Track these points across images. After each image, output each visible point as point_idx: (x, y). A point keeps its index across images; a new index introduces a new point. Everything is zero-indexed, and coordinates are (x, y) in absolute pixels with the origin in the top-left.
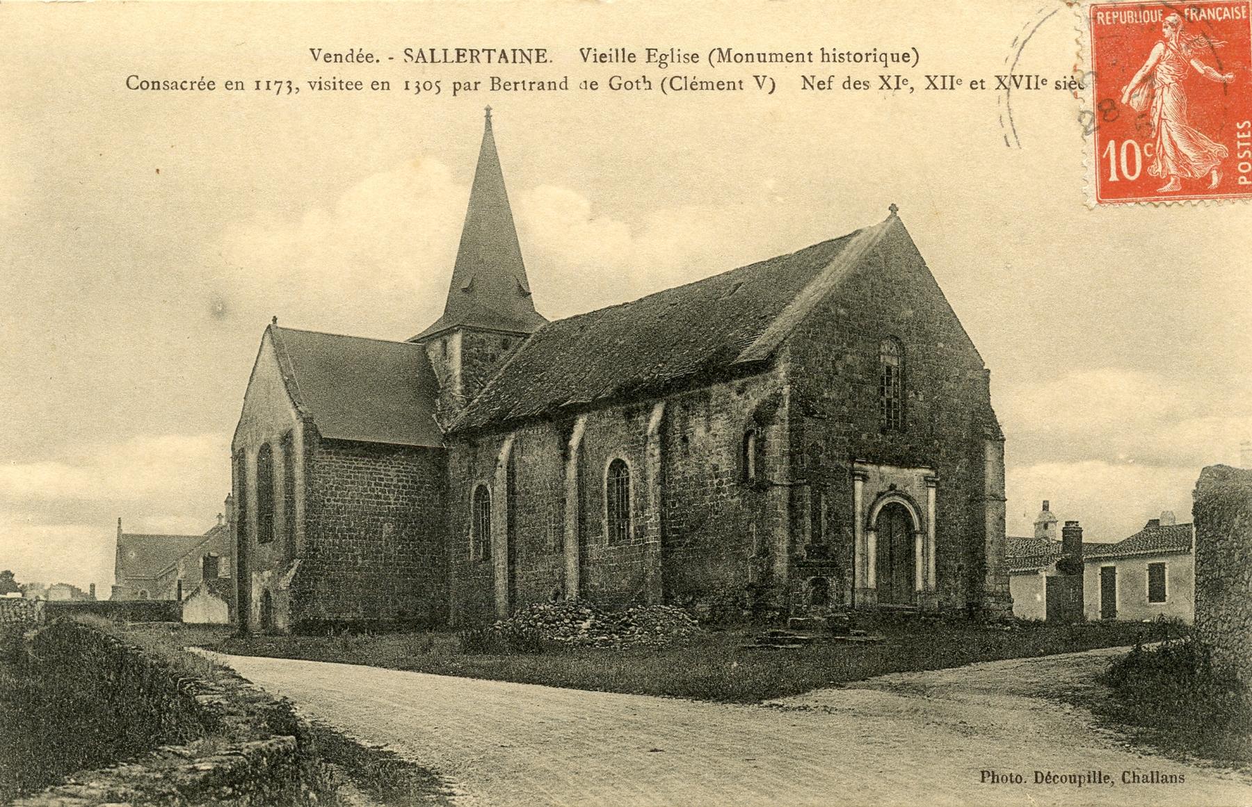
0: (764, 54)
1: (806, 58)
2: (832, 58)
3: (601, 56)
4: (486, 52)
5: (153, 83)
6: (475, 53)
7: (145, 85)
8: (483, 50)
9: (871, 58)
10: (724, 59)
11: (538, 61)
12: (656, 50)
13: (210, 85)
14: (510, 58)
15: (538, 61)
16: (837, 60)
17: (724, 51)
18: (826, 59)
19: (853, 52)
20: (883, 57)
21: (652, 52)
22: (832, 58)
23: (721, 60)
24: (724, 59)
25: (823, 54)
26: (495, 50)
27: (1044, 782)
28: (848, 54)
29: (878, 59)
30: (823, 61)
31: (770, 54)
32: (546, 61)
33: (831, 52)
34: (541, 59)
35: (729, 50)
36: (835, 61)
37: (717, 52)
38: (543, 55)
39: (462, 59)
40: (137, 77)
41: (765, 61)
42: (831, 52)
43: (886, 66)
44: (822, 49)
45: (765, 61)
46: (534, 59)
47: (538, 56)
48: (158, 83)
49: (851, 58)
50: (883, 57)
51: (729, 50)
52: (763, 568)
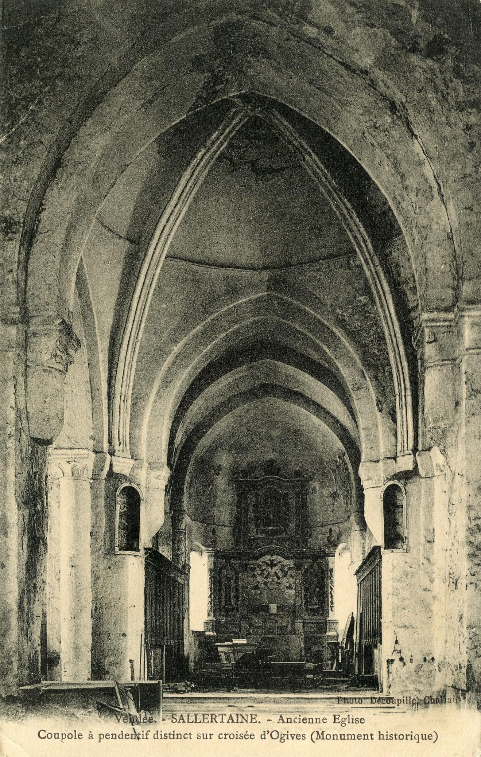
0: (344, 735)
1: (370, 737)
2: (385, 737)
3: (303, 720)
4: (221, 716)
5: (425, 739)
6: (214, 717)
7: (49, 736)
8: (219, 715)
9: (409, 737)
10: (320, 737)
11: (251, 722)
12: (339, 715)
13: (381, 737)
14: (235, 719)
15: (251, 722)
16: (388, 738)
17: (320, 733)
18: (382, 737)
19: (398, 734)
20: (417, 737)
21: (337, 717)
22: (385, 737)
23: (318, 738)
24: (320, 737)
25: (380, 735)
26: (226, 715)
27: (279, 739)
28: (395, 735)
29: (413, 738)
30: (380, 739)
31: (348, 735)
32: (256, 722)
33: (385, 734)
34: (254, 720)
35: (323, 732)
36: (161, 738)
37: (316, 733)
38: (255, 718)
39: (206, 720)
40: (45, 731)
41: (207, 738)
42: (385, 734)
43: (418, 742)
44: (379, 732)
45: (207, 738)
46: (249, 720)
47: (252, 718)
48: (116, 735)
49: (397, 737)
50: (417, 736)
51: (323, 732)
52: (20, 96)
